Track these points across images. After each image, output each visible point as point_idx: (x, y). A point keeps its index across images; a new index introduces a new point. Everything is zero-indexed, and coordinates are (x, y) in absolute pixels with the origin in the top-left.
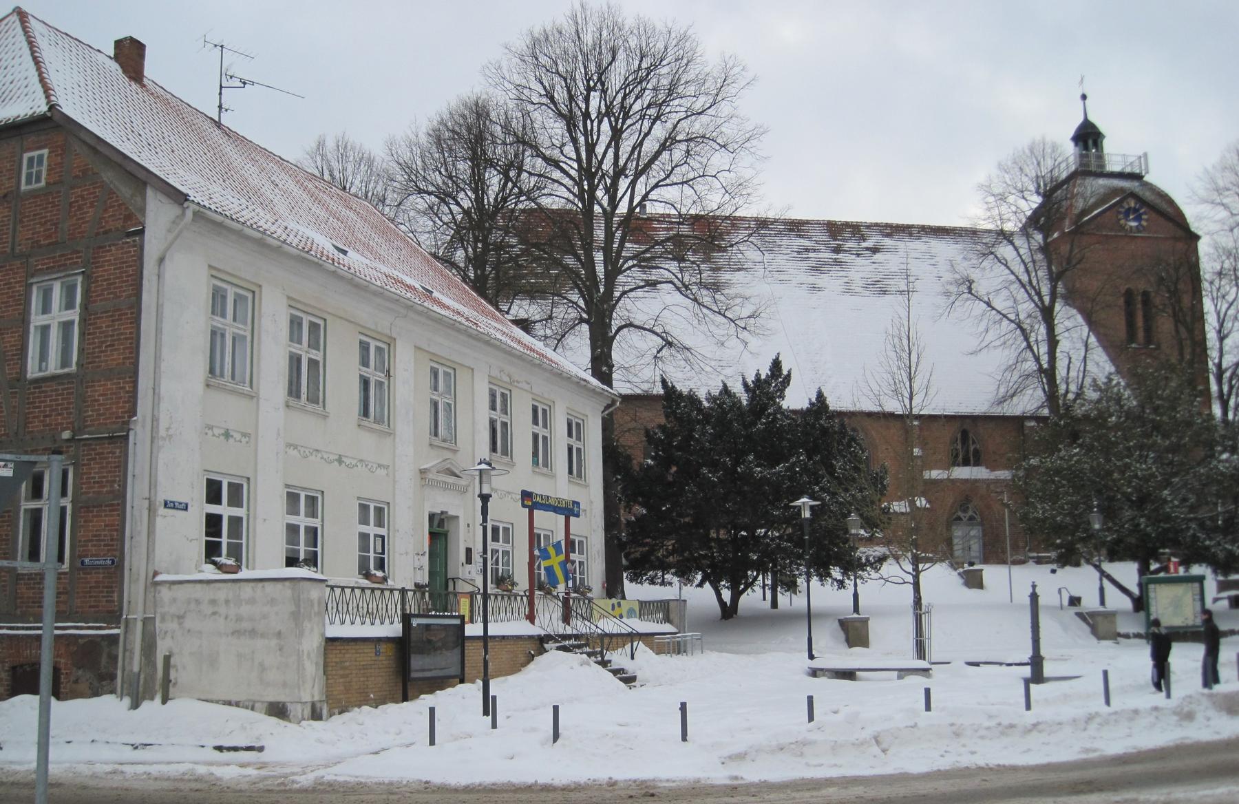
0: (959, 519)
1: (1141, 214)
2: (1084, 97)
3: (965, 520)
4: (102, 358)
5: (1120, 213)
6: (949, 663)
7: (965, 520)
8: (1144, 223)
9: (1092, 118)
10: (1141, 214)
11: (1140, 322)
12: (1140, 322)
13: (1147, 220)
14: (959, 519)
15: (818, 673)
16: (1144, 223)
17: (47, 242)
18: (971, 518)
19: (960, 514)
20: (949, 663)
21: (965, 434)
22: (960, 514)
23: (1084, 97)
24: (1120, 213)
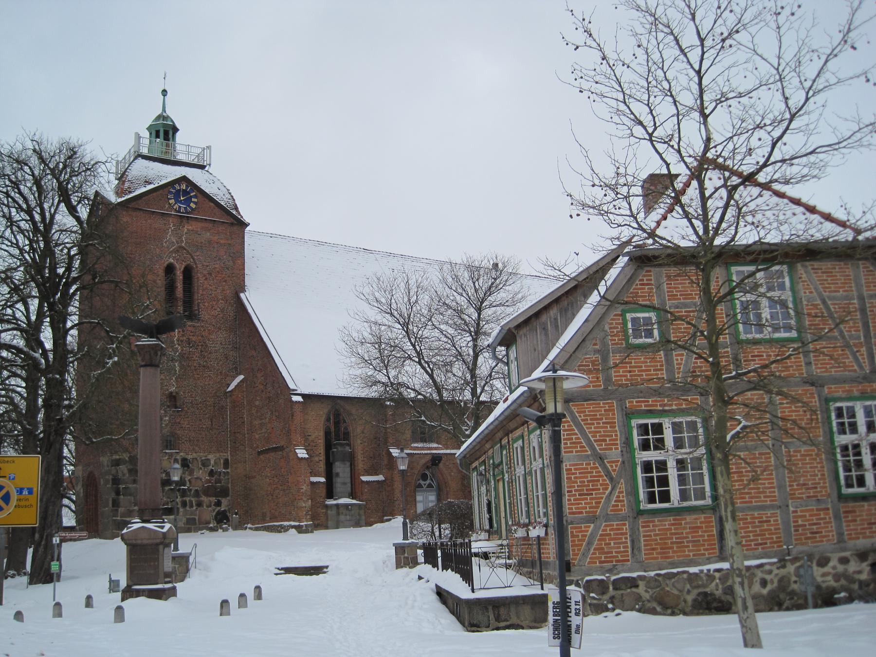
0: (420, 486)
1: (191, 197)
2: (164, 92)
3: (425, 487)
4: (822, 525)
5: (171, 193)
6: (288, 570)
7: (425, 487)
8: (193, 205)
9: (169, 112)
10: (191, 197)
11: (180, 286)
12: (180, 286)
13: (195, 203)
14: (420, 486)
15: (258, 590)
16: (193, 205)
17: (661, 408)
18: (430, 486)
19: (422, 482)
20: (288, 570)
21: (337, 415)
22: (422, 482)
23: (164, 92)
24: (171, 193)
